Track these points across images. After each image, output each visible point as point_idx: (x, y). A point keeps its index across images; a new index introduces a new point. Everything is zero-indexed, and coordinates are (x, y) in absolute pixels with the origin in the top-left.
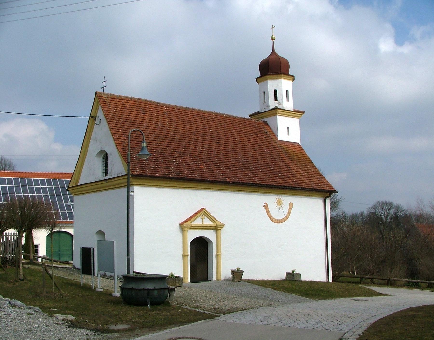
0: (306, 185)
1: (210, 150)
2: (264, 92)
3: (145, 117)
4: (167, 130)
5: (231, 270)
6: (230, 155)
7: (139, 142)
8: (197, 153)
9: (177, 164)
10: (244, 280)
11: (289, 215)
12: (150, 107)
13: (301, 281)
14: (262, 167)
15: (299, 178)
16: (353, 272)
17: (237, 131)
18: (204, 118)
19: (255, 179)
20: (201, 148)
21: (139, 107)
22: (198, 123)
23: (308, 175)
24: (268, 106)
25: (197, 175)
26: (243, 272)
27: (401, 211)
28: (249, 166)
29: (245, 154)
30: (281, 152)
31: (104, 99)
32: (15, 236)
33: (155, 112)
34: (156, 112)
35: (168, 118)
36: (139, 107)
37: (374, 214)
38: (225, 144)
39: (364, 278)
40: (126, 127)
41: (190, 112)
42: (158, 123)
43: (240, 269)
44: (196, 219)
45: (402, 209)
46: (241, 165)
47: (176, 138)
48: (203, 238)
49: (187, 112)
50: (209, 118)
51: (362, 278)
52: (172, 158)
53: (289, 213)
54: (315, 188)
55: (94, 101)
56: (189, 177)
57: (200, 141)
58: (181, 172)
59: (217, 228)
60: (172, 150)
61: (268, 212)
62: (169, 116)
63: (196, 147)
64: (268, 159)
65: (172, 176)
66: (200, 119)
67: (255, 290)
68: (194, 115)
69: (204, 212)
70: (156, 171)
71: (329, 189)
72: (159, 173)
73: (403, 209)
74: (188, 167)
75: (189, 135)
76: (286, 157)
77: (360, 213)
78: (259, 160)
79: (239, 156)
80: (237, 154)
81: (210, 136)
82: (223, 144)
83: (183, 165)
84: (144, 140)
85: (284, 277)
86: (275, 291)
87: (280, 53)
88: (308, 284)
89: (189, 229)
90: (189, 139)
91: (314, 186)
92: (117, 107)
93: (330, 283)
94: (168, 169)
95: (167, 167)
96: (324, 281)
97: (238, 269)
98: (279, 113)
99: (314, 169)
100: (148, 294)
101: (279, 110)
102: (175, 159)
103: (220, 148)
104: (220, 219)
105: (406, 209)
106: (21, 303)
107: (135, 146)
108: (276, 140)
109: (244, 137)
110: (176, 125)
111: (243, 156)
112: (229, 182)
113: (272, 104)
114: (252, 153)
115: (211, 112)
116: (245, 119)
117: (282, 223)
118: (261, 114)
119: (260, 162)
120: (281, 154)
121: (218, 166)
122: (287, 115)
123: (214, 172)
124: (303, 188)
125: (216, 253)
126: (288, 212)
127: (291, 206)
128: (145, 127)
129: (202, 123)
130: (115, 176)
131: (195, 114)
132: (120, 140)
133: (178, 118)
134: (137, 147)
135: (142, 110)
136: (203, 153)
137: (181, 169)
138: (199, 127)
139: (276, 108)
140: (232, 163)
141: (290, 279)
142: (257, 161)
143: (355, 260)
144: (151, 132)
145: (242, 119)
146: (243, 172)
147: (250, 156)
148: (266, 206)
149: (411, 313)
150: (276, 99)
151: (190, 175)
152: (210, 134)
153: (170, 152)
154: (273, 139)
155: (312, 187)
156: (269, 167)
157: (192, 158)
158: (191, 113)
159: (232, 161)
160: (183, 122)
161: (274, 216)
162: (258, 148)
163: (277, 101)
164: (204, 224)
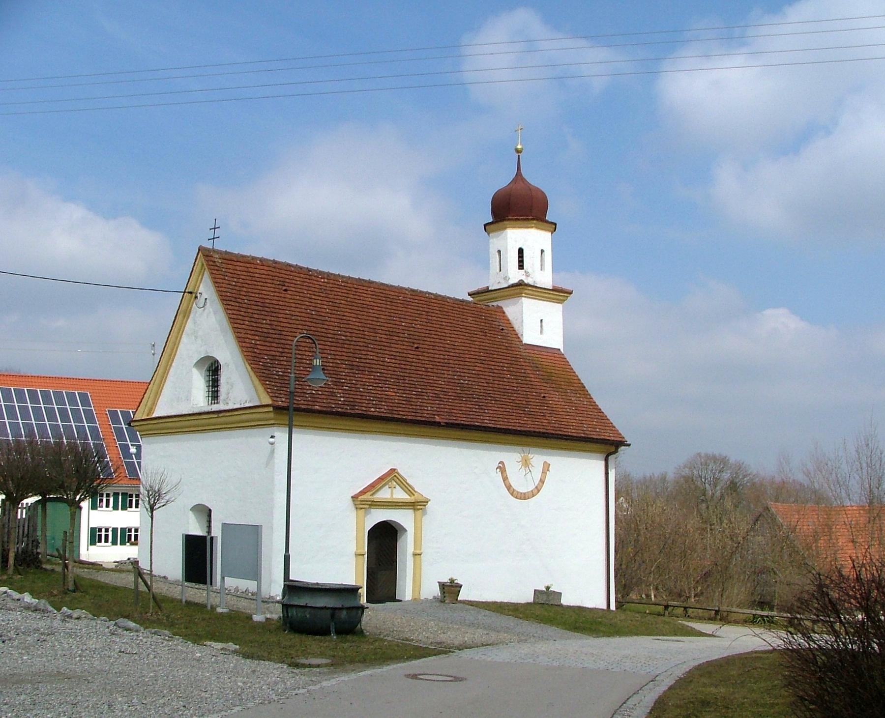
0: (573, 431)
1: (402, 362)
2: (499, 252)
3: (289, 296)
4: (327, 323)
5: (439, 582)
6: (439, 371)
7: (280, 345)
8: (382, 367)
9: (349, 387)
10: (460, 601)
11: (541, 484)
12: (295, 278)
13: (561, 605)
14: (495, 396)
15: (561, 417)
16: (648, 596)
17: (449, 325)
18: (390, 300)
19: (485, 418)
20: (388, 358)
21: (276, 278)
22: (380, 309)
23: (577, 411)
24: (506, 278)
25: (383, 411)
26: (461, 586)
27: (745, 476)
28: (473, 393)
29: (465, 371)
30: (527, 368)
31: (215, 262)
32: (25, 508)
33: (304, 287)
34: (307, 288)
35: (327, 299)
36: (276, 278)
37: (689, 480)
38: (429, 351)
39: (671, 606)
40: (255, 316)
41: (365, 288)
42: (311, 308)
43: (455, 582)
44: (381, 488)
45: (746, 471)
46: (459, 391)
47: (344, 338)
48: (391, 523)
49: (360, 287)
50: (399, 300)
51: (666, 607)
52: (339, 377)
53: (542, 481)
54: (589, 436)
55: (195, 263)
56: (371, 413)
57: (385, 344)
58: (357, 404)
59: (417, 505)
60: (338, 361)
61: (505, 479)
62: (330, 296)
63: (379, 355)
64: (505, 380)
65: (343, 410)
66: (384, 302)
67: (485, 617)
68: (373, 293)
69: (395, 476)
70: (314, 400)
71: (616, 439)
72: (320, 404)
73: (749, 472)
74: (368, 394)
75: (366, 333)
76: (537, 376)
77: (658, 476)
78: (489, 381)
79: (455, 373)
80: (450, 369)
81: (401, 335)
82: (426, 350)
83: (358, 390)
84: (318, 353)
85: (530, 598)
86: (521, 621)
87: (535, 178)
88: (574, 612)
89: (367, 506)
90: (367, 341)
91: (587, 432)
92: (238, 277)
93: (612, 611)
94: (335, 398)
95: (333, 394)
96: (600, 607)
97: (452, 581)
98: (525, 294)
99: (587, 400)
100: (333, 616)
101: (526, 287)
102: (344, 377)
103: (420, 357)
104: (422, 489)
105: (755, 472)
106: (134, 624)
107: (273, 353)
108: (518, 343)
109: (462, 337)
110: (342, 313)
111: (462, 374)
112: (440, 423)
113: (515, 276)
114: (477, 368)
115: (402, 288)
116: (463, 301)
117: (528, 498)
118: (492, 293)
119: (491, 385)
120: (529, 372)
121: (418, 393)
122: (540, 296)
123: (413, 403)
124: (569, 436)
125: (413, 550)
126: (541, 479)
127: (546, 467)
128: (288, 316)
129: (387, 310)
130: (236, 407)
131: (375, 292)
132: (247, 340)
133: (346, 299)
134: (278, 354)
135: (281, 283)
136: (392, 367)
137: (357, 397)
138: (383, 317)
139: (521, 284)
140: (443, 386)
141: (542, 602)
142: (486, 385)
143: (653, 571)
144: (300, 327)
145: (459, 302)
146: (463, 405)
147: (473, 374)
148: (502, 468)
149: (754, 655)
150: (521, 266)
151: (372, 409)
152: (402, 332)
153: (334, 365)
154: (513, 342)
155: (584, 434)
156: (508, 394)
157: (372, 377)
158: (367, 291)
159: (443, 383)
160: (354, 308)
161: (515, 485)
162: (487, 359)
163: (523, 269)
164: (394, 497)
